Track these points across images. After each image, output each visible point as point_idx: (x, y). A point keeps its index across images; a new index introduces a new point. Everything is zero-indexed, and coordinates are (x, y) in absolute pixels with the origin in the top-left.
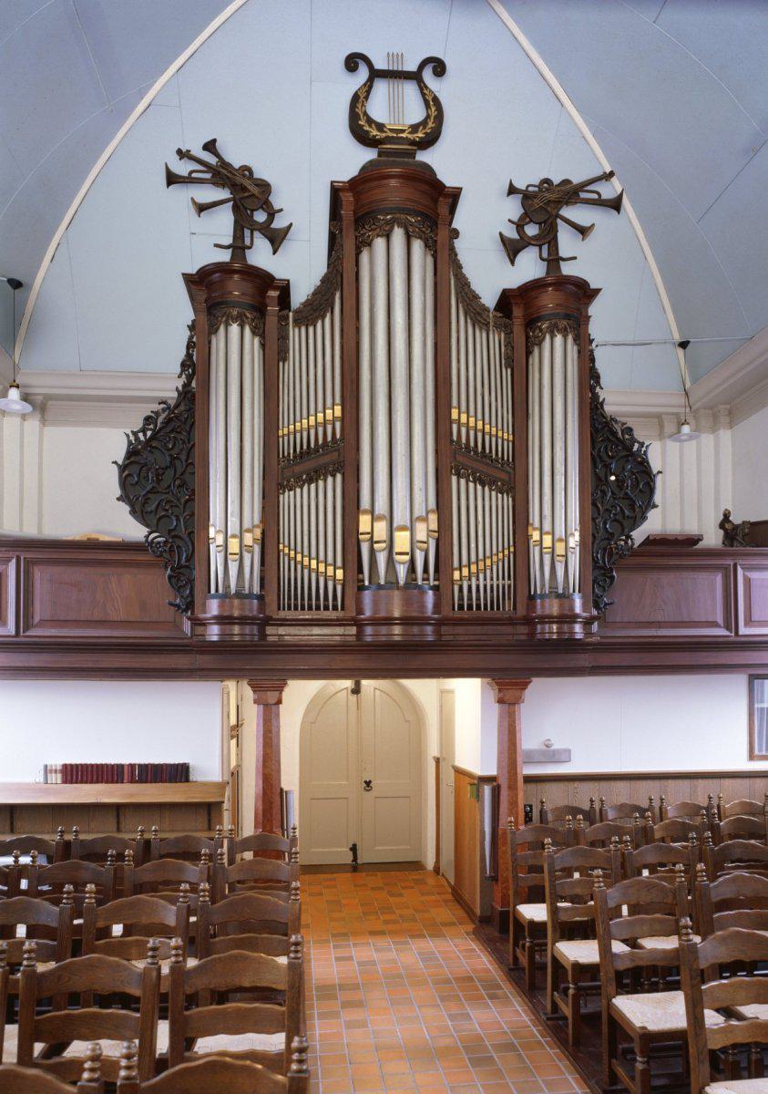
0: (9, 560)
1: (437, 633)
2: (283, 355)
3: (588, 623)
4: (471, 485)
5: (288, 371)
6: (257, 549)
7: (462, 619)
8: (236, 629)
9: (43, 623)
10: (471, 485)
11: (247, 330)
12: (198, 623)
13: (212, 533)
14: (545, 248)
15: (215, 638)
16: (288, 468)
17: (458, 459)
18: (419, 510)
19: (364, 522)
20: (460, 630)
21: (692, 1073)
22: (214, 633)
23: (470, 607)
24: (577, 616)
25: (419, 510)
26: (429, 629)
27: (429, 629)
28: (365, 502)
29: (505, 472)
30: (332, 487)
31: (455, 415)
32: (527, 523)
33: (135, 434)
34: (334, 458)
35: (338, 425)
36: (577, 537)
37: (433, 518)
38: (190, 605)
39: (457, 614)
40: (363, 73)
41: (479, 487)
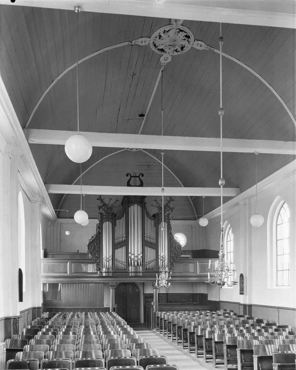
0: (68, 262)
1: (142, 274)
2: (115, 225)
3: (143, 273)
4: (148, 248)
5: (116, 228)
6: (111, 260)
7: (151, 272)
8: (133, 274)
9: (74, 273)
10: (148, 248)
11: (110, 222)
12: (102, 273)
13: (104, 257)
14: (169, 204)
15: (104, 275)
16: (115, 246)
17: (145, 243)
18: (110, 256)
19: (130, 255)
20: (147, 274)
21: (32, 313)
22: (104, 274)
23: (123, 270)
24: (167, 271)
25: (110, 256)
26: (141, 274)
27: (141, 274)
28: (130, 251)
29: (155, 246)
30: (124, 248)
31: (145, 235)
32: (158, 255)
33: (90, 240)
34: (125, 243)
35: (125, 238)
36: (167, 257)
37: (141, 254)
38: (99, 270)
39: (118, 271)
40: (129, 177)
41: (150, 248)
